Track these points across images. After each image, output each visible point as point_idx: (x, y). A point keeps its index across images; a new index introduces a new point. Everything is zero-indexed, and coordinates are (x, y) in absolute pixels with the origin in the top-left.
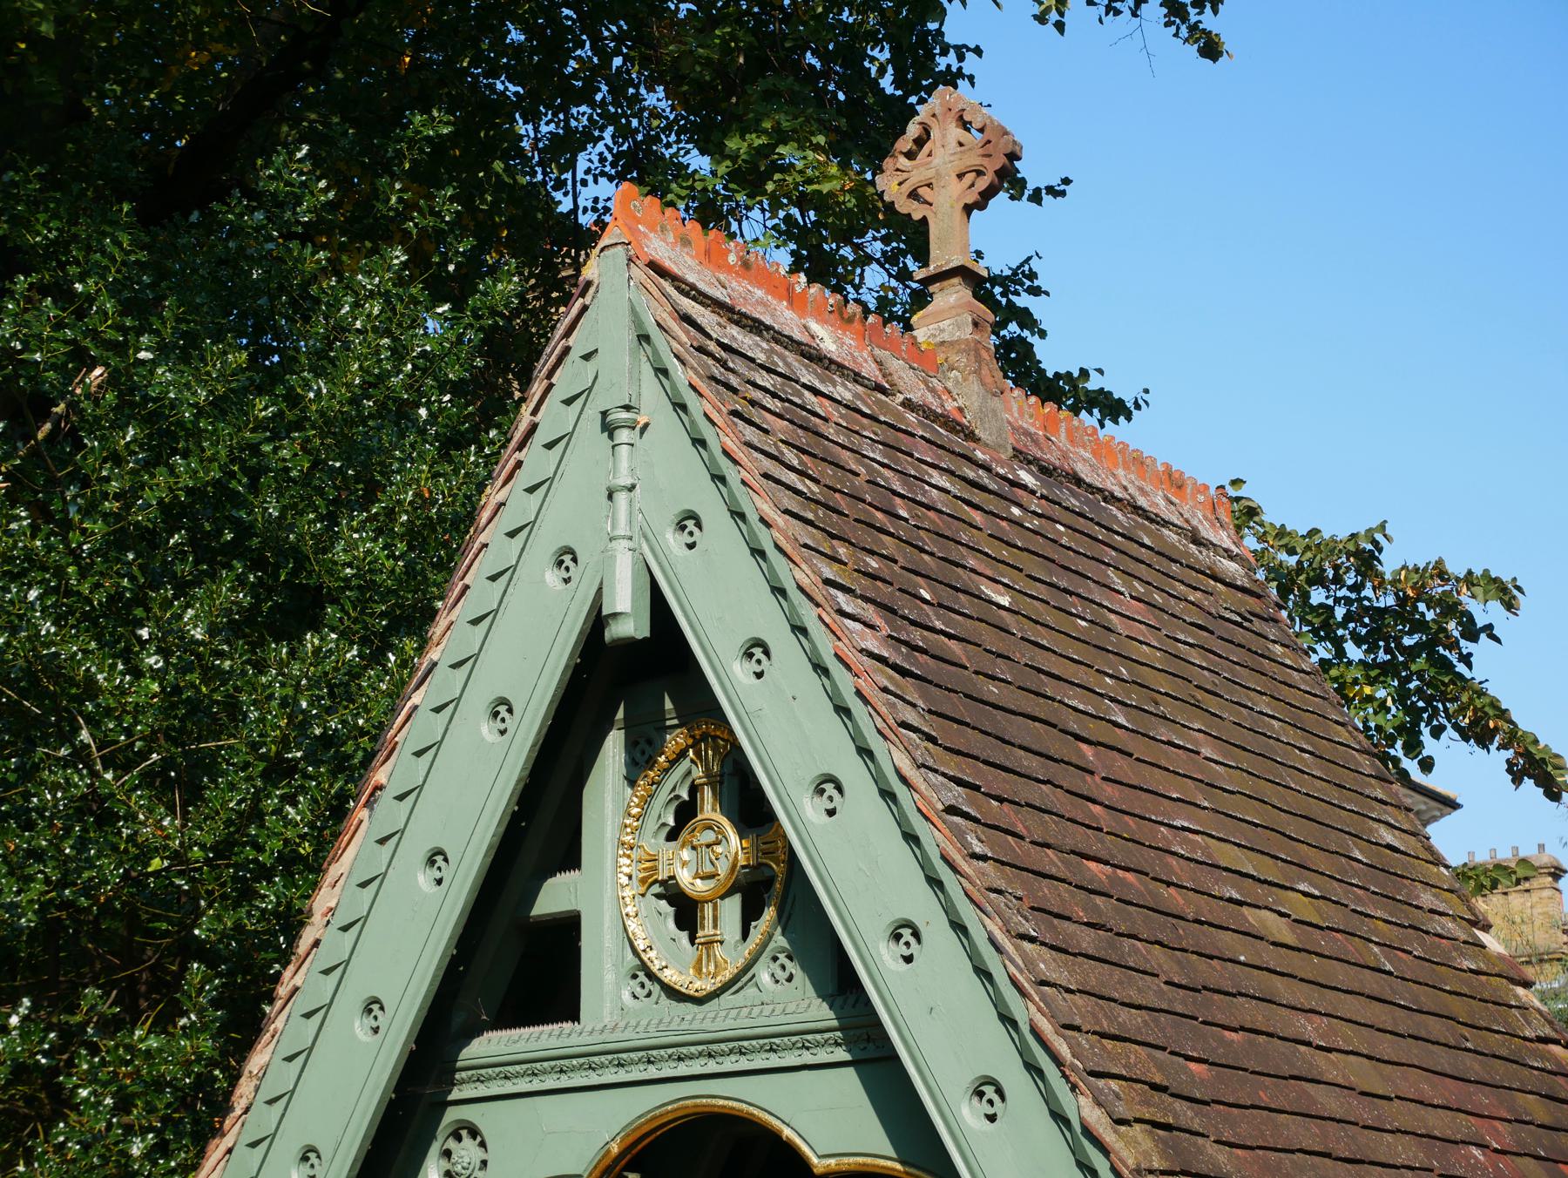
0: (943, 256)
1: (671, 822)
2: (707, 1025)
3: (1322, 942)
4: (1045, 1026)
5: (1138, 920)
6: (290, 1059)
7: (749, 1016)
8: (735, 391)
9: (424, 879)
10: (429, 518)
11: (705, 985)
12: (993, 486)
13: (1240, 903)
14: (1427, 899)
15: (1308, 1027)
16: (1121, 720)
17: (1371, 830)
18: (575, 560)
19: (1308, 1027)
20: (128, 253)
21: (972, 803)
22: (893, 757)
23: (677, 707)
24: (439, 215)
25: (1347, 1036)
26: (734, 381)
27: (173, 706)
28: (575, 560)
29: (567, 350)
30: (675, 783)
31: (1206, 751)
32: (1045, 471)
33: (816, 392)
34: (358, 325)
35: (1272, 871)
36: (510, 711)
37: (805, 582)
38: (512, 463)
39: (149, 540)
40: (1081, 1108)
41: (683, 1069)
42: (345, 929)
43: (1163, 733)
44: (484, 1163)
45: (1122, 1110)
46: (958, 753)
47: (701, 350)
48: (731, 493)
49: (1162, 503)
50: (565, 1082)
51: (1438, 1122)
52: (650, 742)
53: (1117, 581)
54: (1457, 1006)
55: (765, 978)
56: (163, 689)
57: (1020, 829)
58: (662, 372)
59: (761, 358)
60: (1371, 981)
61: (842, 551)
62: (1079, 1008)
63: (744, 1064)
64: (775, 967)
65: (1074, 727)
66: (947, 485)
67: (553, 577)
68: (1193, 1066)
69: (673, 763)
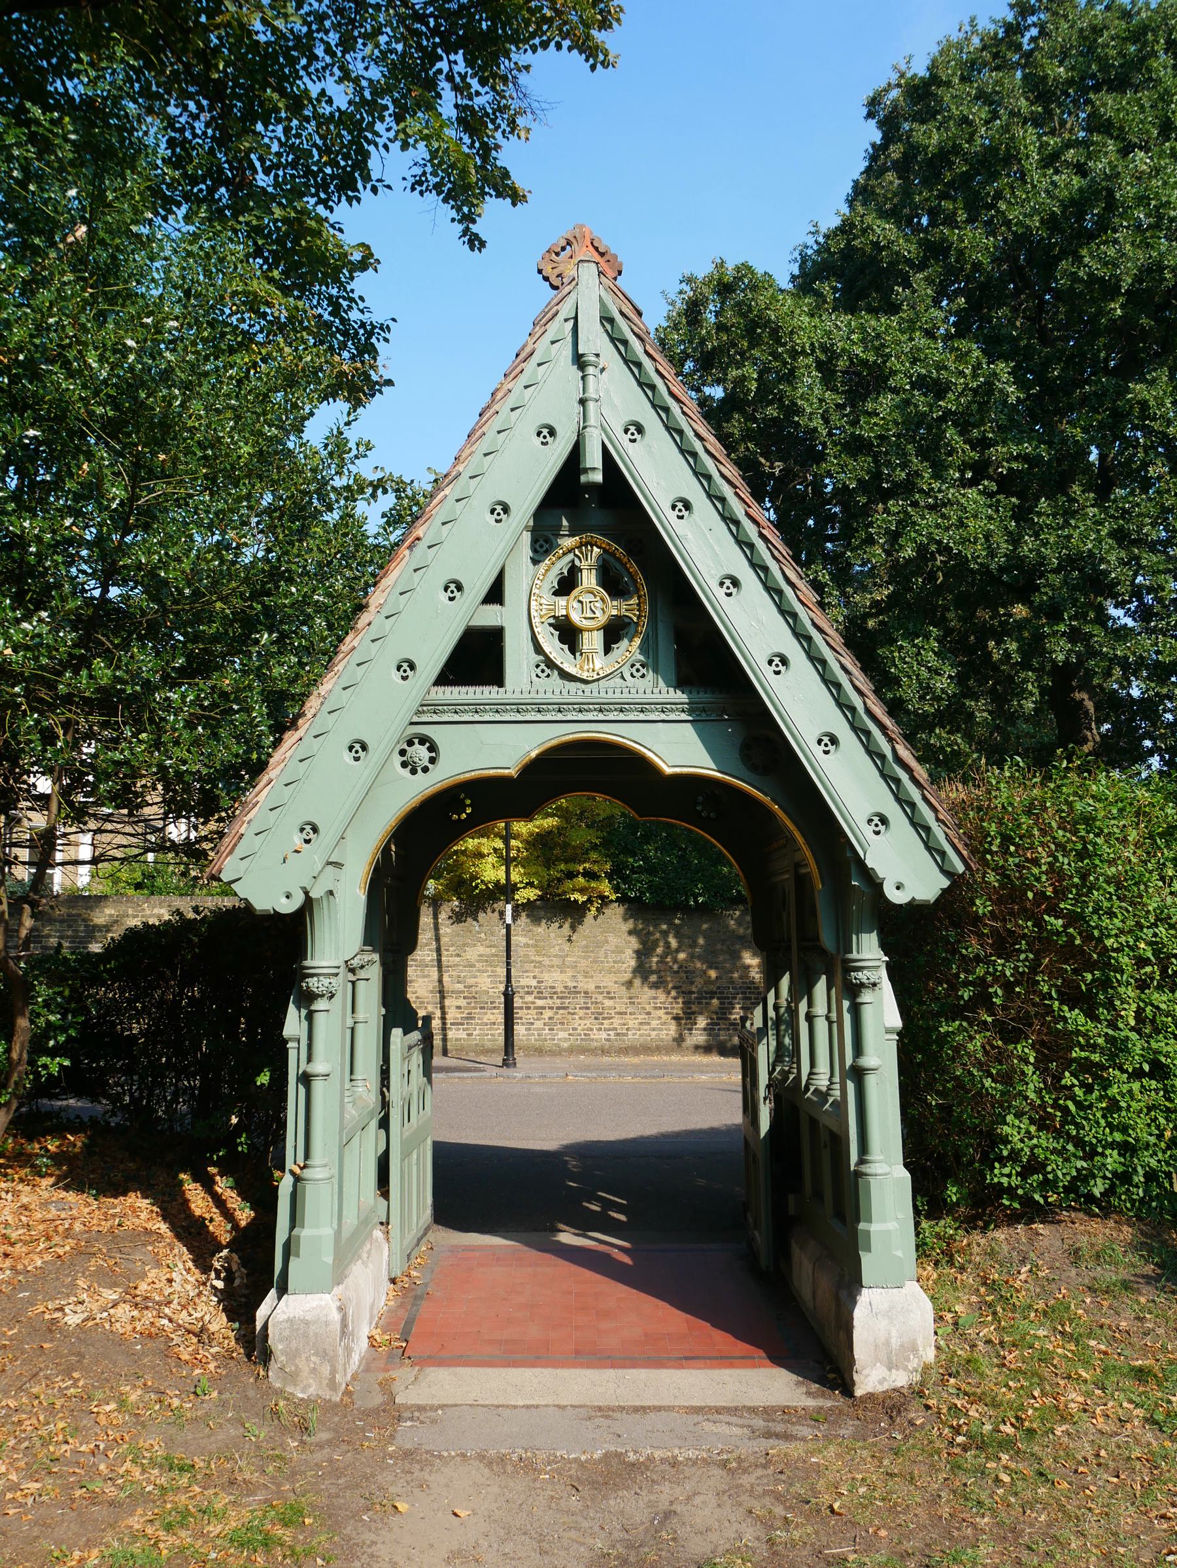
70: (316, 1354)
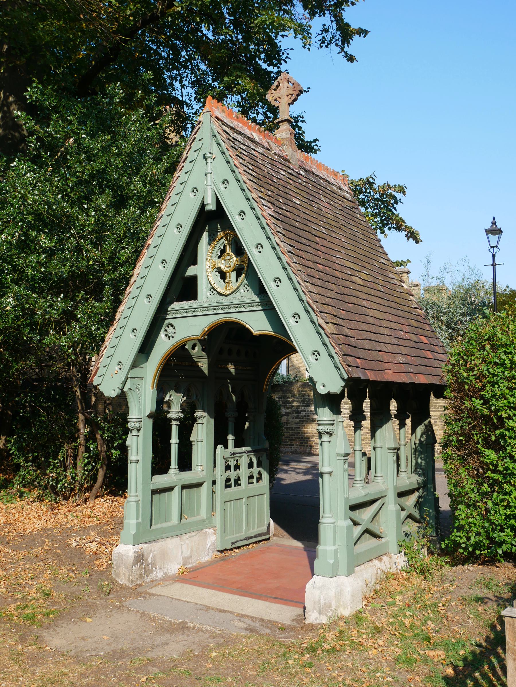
0: (282, 116)
1: (219, 254)
2: (228, 301)
3: (369, 284)
4: (310, 302)
5: (329, 278)
6: (129, 308)
7: (238, 299)
8: (237, 150)
9: (161, 267)
10: (155, 179)
11: (229, 292)
12: (295, 175)
13: (351, 275)
14: (391, 275)
15: (366, 303)
16: (325, 232)
17: (379, 259)
18: (197, 191)
19: (366, 303)
20: (81, 110)
21: (293, 250)
22: (275, 239)
23: (221, 227)
24: (151, 101)
25: (374, 306)
26: (236, 147)
27: (98, 224)
28: (197, 191)
29: (195, 138)
30: (220, 245)
31: (343, 240)
32: (306, 171)
33: (255, 150)
34: (133, 129)
35: (358, 268)
36: (181, 227)
37: (254, 197)
38: (181, 166)
39: (87, 183)
40: (319, 320)
41: (222, 311)
42: (142, 278)
43: (334, 235)
44: (175, 333)
45: (327, 320)
46: (290, 239)
47: (229, 139)
48: (236, 175)
49: (332, 179)
50: (194, 314)
51: (393, 325)
52: (214, 235)
53: (323, 198)
54: (397, 300)
55: (242, 290)
56: (95, 220)
57: (304, 257)
58: (219, 144)
59: (242, 141)
60: (379, 294)
61: (263, 190)
62: (318, 298)
63: (237, 310)
64: (244, 288)
65: (314, 233)
66: (285, 174)
67: (192, 195)
68: (342, 311)
69: (220, 240)
70: (125, 568)
